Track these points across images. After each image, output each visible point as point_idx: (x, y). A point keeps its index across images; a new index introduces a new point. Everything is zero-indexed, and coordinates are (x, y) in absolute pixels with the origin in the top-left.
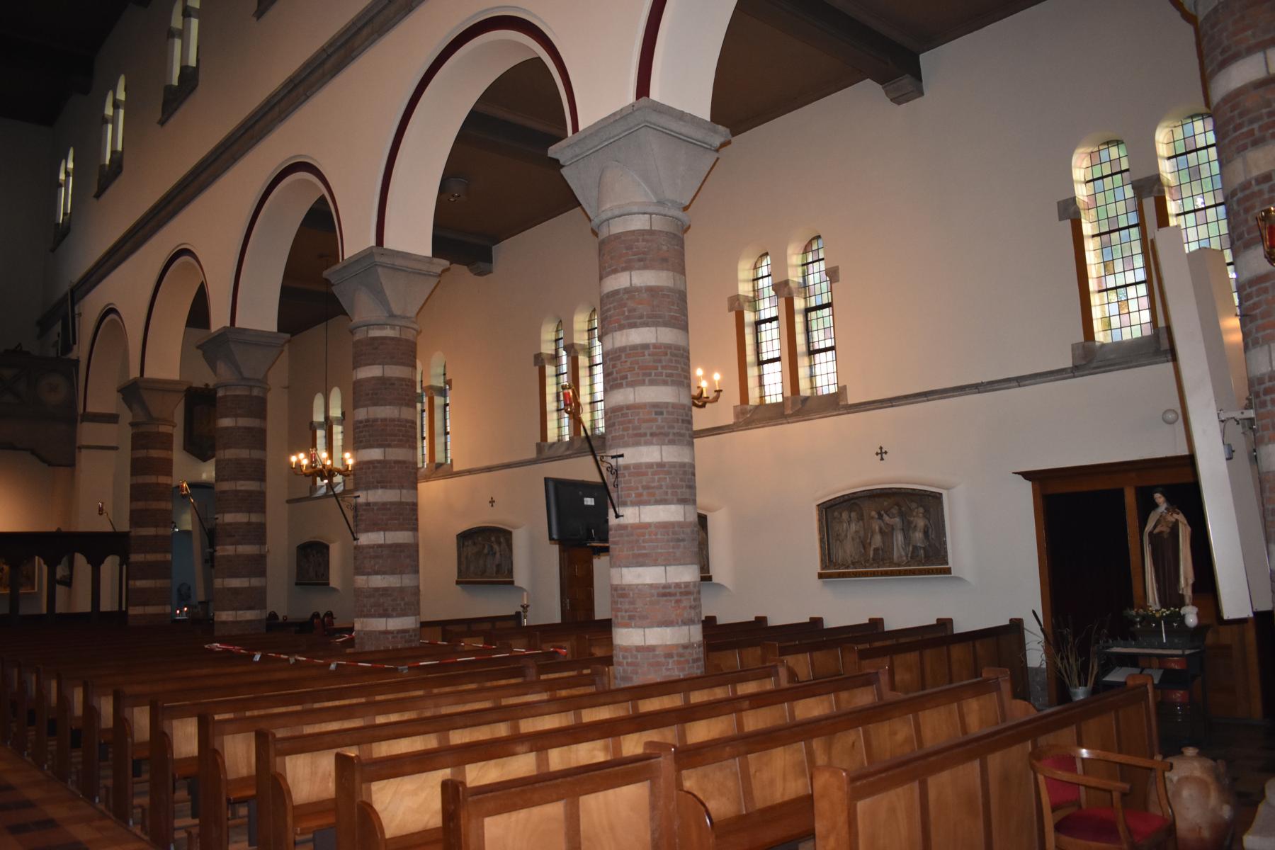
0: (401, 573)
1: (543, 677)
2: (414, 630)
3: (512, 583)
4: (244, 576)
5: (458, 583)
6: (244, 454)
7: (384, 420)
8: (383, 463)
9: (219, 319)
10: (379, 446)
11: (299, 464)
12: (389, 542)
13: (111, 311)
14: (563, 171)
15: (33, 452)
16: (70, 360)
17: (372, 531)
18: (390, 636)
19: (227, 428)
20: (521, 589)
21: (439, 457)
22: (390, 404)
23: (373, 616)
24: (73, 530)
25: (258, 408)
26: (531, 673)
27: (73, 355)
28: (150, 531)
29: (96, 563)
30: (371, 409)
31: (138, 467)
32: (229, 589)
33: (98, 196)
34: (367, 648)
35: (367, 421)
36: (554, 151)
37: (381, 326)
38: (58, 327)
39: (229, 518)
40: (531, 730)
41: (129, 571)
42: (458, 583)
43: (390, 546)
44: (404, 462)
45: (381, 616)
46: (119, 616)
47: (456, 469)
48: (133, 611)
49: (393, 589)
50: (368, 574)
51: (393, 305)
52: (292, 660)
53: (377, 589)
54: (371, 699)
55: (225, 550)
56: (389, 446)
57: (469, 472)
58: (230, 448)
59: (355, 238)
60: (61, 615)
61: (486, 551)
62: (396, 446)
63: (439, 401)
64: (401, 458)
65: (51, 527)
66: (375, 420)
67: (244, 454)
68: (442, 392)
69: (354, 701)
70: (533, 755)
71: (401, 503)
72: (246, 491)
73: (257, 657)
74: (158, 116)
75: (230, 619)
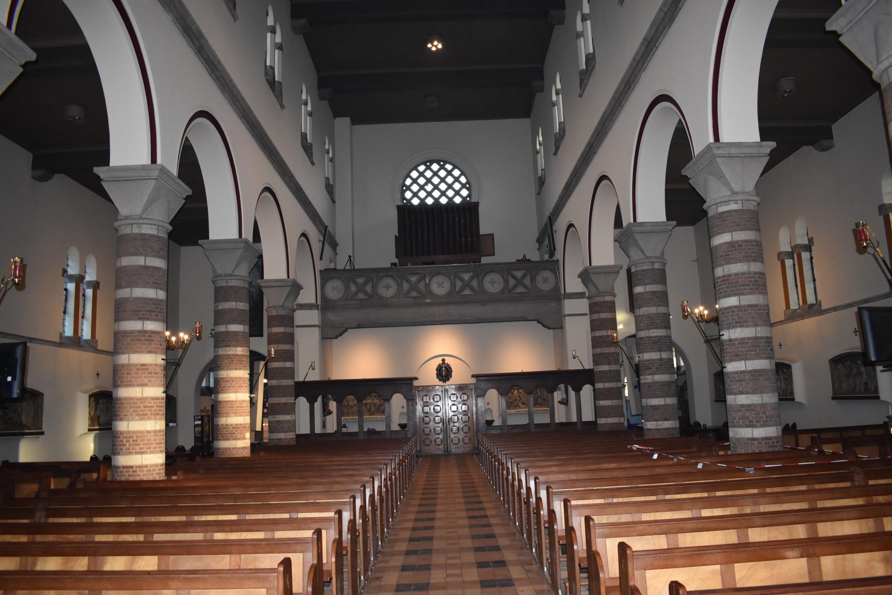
0: (762, 392)
1: (871, 482)
2: (776, 438)
3: (878, 398)
4: (660, 397)
5: (833, 398)
6: (653, 310)
7: (737, 274)
8: (739, 307)
9: (627, 219)
10: (735, 295)
11: (702, 316)
12: (749, 368)
13: (571, 225)
14: (841, 39)
15: (539, 322)
16: (553, 261)
17: (736, 360)
18: (756, 442)
19: (640, 293)
20: (886, 403)
21: (811, 299)
22: (740, 262)
23: (742, 426)
24: (566, 369)
25: (661, 276)
26: (859, 479)
27: (555, 258)
28: (605, 368)
29: (578, 390)
30: (726, 267)
31: (595, 325)
32: (651, 406)
33: (555, 154)
34: (738, 452)
35: (724, 276)
36: (834, 24)
37: (727, 202)
38: (546, 242)
39: (647, 356)
40: (830, 534)
41: (597, 395)
42: (833, 398)
43: (750, 372)
44: (756, 305)
45: (747, 426)
46: (594, 423)
47: (824, 307)
48: (601, 421)
49: (756, 405)
50: (735, 394)
51: (733, 185)
52: (675, 460)
53: (742, 406)
54: (712, 494)
55: (647, 379)
56: (743, 294)
57: (835, 309)
58: (642, 307)
59: (700, 139)
60: (561, 424)
61: (854, 371)
62: (748, 294)
63: (805, 255)
64: (753, 302)
65: (553, 368)
66: (730, 275)
67: (653, 310)
68: (808, 248)
69: (75, 520)
70: (804, 560)
71: (756, 338)
72: (656, 337)
73: (655, 456)
74: (578, 91)
75: (653, 427)
